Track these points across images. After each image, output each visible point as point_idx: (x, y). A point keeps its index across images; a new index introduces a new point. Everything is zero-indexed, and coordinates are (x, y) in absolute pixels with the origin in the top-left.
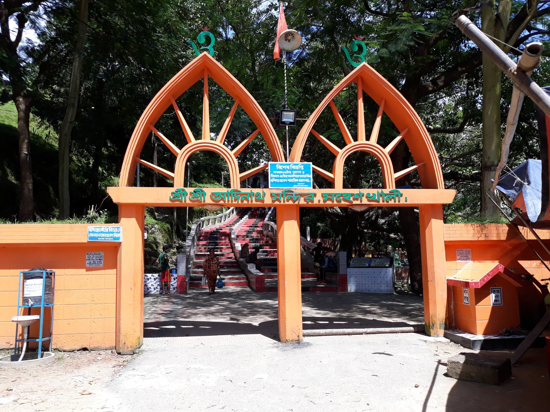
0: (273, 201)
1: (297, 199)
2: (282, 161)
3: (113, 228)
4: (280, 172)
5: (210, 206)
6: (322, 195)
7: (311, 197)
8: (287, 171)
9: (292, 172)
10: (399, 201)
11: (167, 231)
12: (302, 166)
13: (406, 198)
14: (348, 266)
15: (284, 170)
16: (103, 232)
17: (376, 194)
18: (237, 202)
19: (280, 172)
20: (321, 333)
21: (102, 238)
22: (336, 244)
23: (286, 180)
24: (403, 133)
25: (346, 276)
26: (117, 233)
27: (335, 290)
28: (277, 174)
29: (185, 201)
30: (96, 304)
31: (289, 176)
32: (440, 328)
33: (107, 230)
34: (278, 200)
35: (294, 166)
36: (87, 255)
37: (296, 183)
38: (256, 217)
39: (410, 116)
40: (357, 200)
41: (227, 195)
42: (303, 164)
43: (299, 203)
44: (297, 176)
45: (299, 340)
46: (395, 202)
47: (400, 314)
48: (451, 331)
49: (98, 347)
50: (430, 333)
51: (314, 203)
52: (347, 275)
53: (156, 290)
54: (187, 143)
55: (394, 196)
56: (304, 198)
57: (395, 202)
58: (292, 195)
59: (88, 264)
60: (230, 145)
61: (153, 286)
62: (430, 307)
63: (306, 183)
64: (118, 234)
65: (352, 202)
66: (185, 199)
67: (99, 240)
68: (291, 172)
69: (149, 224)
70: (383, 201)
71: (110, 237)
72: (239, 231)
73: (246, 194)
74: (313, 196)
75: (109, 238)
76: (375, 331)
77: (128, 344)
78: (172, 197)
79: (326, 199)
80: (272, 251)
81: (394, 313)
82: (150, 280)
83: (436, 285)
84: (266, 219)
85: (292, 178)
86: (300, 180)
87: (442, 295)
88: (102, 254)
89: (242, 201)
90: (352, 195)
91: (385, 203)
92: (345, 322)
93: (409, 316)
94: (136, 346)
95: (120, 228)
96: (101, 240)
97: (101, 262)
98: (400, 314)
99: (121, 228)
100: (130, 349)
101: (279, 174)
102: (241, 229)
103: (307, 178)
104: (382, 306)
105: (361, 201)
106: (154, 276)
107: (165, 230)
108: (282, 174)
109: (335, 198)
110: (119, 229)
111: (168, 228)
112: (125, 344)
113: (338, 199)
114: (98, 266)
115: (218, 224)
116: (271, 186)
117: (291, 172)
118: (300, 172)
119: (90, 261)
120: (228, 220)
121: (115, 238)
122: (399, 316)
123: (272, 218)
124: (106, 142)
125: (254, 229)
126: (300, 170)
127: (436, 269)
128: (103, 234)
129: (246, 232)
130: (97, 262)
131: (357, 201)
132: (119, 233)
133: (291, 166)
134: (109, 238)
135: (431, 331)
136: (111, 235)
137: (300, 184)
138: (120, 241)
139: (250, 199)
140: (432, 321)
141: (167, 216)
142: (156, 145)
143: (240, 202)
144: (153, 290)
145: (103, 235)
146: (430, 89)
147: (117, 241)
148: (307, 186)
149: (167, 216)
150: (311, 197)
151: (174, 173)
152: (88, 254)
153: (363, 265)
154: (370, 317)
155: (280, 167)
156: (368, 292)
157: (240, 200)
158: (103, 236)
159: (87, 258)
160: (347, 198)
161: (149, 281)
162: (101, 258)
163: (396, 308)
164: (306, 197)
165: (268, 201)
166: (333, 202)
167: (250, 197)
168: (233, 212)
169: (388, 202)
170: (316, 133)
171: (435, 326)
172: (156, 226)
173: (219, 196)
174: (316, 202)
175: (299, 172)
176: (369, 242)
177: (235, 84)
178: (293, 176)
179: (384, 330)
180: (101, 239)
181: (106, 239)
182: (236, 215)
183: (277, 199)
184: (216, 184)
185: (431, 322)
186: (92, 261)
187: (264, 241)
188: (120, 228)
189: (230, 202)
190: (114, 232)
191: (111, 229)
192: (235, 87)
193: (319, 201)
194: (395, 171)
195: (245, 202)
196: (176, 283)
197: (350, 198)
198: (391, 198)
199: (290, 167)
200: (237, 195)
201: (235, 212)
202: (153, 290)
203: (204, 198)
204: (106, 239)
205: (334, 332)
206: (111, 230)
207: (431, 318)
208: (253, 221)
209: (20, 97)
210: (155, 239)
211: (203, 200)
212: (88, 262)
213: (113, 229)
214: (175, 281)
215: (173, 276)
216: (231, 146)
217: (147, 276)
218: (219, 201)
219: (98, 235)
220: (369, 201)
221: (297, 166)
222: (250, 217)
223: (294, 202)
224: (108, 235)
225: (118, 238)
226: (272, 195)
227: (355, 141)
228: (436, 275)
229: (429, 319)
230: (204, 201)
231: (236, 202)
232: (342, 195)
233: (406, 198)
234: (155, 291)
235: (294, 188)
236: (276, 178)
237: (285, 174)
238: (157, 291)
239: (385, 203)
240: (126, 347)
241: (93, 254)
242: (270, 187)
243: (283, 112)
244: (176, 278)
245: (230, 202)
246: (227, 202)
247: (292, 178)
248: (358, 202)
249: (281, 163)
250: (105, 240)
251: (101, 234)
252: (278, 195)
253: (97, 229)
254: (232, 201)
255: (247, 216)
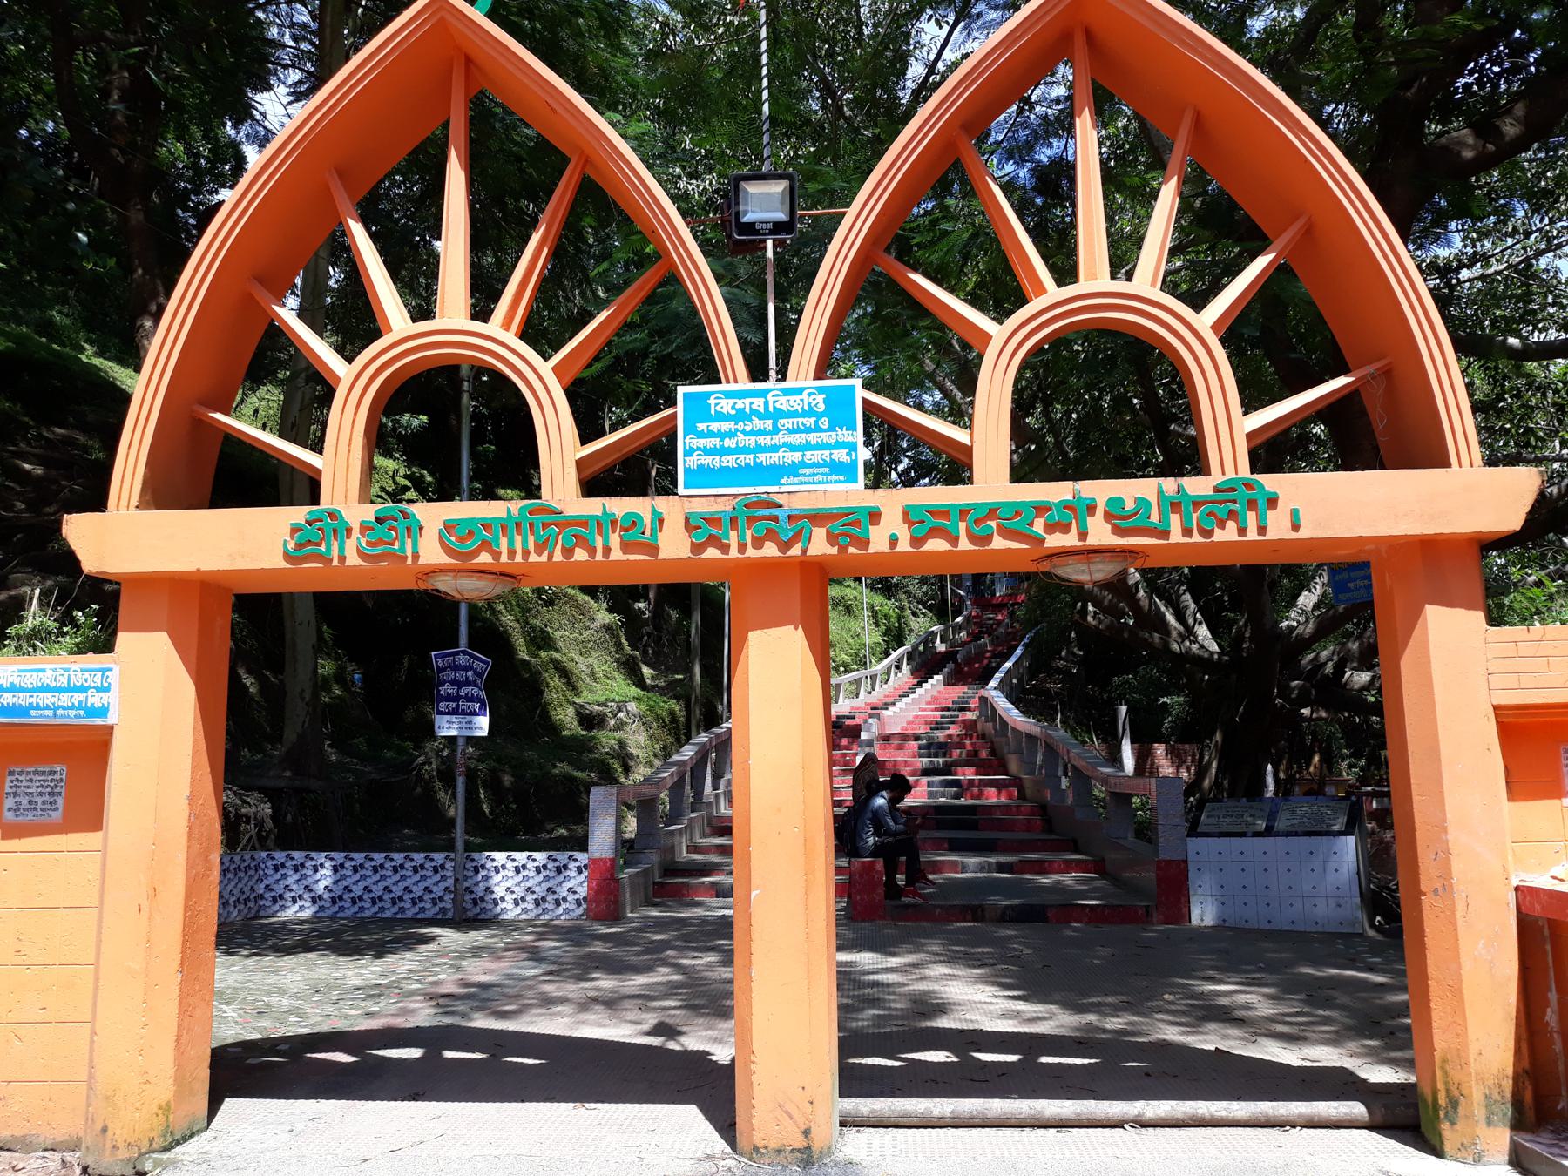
0: (697, 548)
1: (797, 537)
2: (736, 381)
3: (87, 670)
4: (725, 426)
5: (448, 578)
6: (906, 514)
7: (856, 523)
8: (756, 421)
9: (775, 425)
10: (1262, 530)
11: (667, 720)
12: (820, 398)
13: (1294, 513)
14: (1193, 831)
15: (741, 416)
16: (46, 689)
17: (1153, 500)
18: (546, 554)
19: (725, 426)
20: (936, 1113)
21: (44, 709)
22: (1206, 758)
23: (750, 458)
24: (1279, 243)
25: (1182, 866)
26: (98, 689)
27: (1145, 918)
28: (710, 434)
29: (342, 559)
30: (29, 966)
31: (765, 440)
32: (1489, 1123)
33: (63, 681)
34: (713, 541)
35: (783, 400)
36: (9, 778)
37: (792, 470)
38: (970, 680)
39: (1306, 160)
40: (1066, 528)
41: (504, 528)
42: (820, 390)
43: (804, 551)
44: (799, 439)
45: (809, 1148)
46: (1242, 531)
47: (1348, 1028)
48: (1546, 1137)
49: (24, 1136)
50: (1442, 1143)
51: (872, 550)
52: (1186, 862)
53: (522, 905)
54: (376, 334)
55: (1232, 506)
56: (828, 531)
57: (1242, 531)
58: (775, 519)
59: (9, 810)
60: (896, 470)
61: (513, 892)
62: (1435, 1015)
63: (836, 468)
64: (101, 694)
65: (1043, 541)
66: (342, 549)
67: (35, 718)
68: (769, 422)
69: (613, 700)
70: (1187, 532)
71: (73, 707)
72: (909, 723)
73: (583, 522)
74: (865, 520)
75: (69, 708)
76: (1180, 1116)
77: (118, 1132)
78: (291, 545)
79: (921, 530)
80: (977, 783)
81: (1326, 1021)
82: (503, 873)
83: (1459, 914)
84: (993, 683)
85: (774, 448)
86: (808, 454)
87: (1491, 962)
88: (62, 771)
89: (568, 552)
90: (1041, 509)
91: (1196, 538)
92: (1086, 1061)
93: (1382, 1038)
94: (151, 1141)
95: (111, 670)
96: (41, 716)
97: (56, 802)
98: (1348, 1028)
99: (116, 669)
100: (123, 1154)
101: (721, 435)
102: (917, 717)
103: (839, 445)
104: (1288, 987)
105: (1083, 535)
106: (514, 860)
107: (658, 718)
108: (732, 434)
109: (962, 526)
110: (108, 673)
111: (672, 713)
112: (105, 1130)
113: (976, 530)
114: (45, 819)
115: (848, 701)
116: (686, 487)
117: (769, 422)
118: (810, 422)
119: (17, 799)
120: (880, 692)
121: (92, 711)
122: (1335, 1041)
123: (1015, 681)
124: (529, 474)
125: (958, 716)
126: (809, 412)
127: (1457, 838)
128: (49, 695)
129: (929, 726)
130: (44, 803)
131: (1065, 536)
132: (107, 690)
133: (770, 398)
134: (69, 708)
135: (1445, 1127)
136: (78, 697)
137: (808, 471)
138: (110, 721)
139: (599, 543)
140: (1446, 1083)
141: (681, 677)
142: (654, 473)
143: (558, 557)
144: (389, 905)
145: (49, 698)
146: (1468, 154)
147: (99, 721)
148: (842, 478)
149: (681, 677)
150: (856, 523)
151: (321, 453)
152: (11, 773)
153: (1248, 824)
154: (1208, 1040)
155: (726, 406)
156: (1268, 927)
157: (559, 547)
158: (47, 701)
159: (8, 790)
160: (1015, 524)
161: (498, 878)
162: (58, 790)
163: (1343, 999)
164: (836, 527)
165: (674, 545)
166: (954, 540)
167: (600, 532)
168: (898, 667)
169: (1207, 533)
170: (890, 264)
171: (1460, 1110)
172: (632, 707)
173: (471, 533)
174: (878, 541)
175: (804, 420)
176: (1350, 757)
177: (552, 96)
178: (779, 439)
179: (1223, 1114)
180: (41, 712)
181: (58, 712)
182: (909, 675)
183: (711, 537)
184: (849, 586)
185: (1440, 1086)
186: (25, 801)
187: (964, 752)
188: (111, 670)
189: (519, 558)
190: (89, 687)
191: (79, 674)
192: (555, 106)
193: (893, 542)
194: (1249, 406)
195: (580, 555)
196: (586, 884)
197: (1031, 524)
198: (1223, 515)
199: (766, 403)
200: (545, 526)
201: (906, 668)
202: (510, 906)
203: (415, 545)
204: (59, 712)
205: (991, 1114)
206: (78, 680)
207: (1442, 1068)
208: (958, 691)
209: (146, 317)
210: (622, 744)
211: (409, 554)
212: (9, 802)
213: (87, 675)
214: (582, 877)
215: (576, 860)
216: (897, 473)
217: (493, 860)
218: (476, 553)
219: (31, 700)
220: (1118, 531)
221: (798, 398)
222: (948, 682)
223: (785, 546)
224: (65, 699)
225: (103, 711)
226: (689, 526)
227: (1060, 283)
228: (1457, 867)
229: (1434, 1072)
230: (416, 556)
231: (544, 558)
232: (993, 512)
233: (1294, 513)
234: (519, 910)
235: (783, 489)
236: (707, 452)
237: (745, 433)
238: (525, 911)
239: (1196, 538)
240: (109, 1145)
241: (28, 773)
242: (681, 490)
243: (743, 184)
244: (585, 866)
245: (519, 558)
246: (504, 558)
247: (774, 448)
248: (1070, 540)
249: (732, 387)
250: (55, 716)
251: (41, 695)
252: (713, 521)
253: (29, 675)
254: (526, 553)
255: (939, 677)
